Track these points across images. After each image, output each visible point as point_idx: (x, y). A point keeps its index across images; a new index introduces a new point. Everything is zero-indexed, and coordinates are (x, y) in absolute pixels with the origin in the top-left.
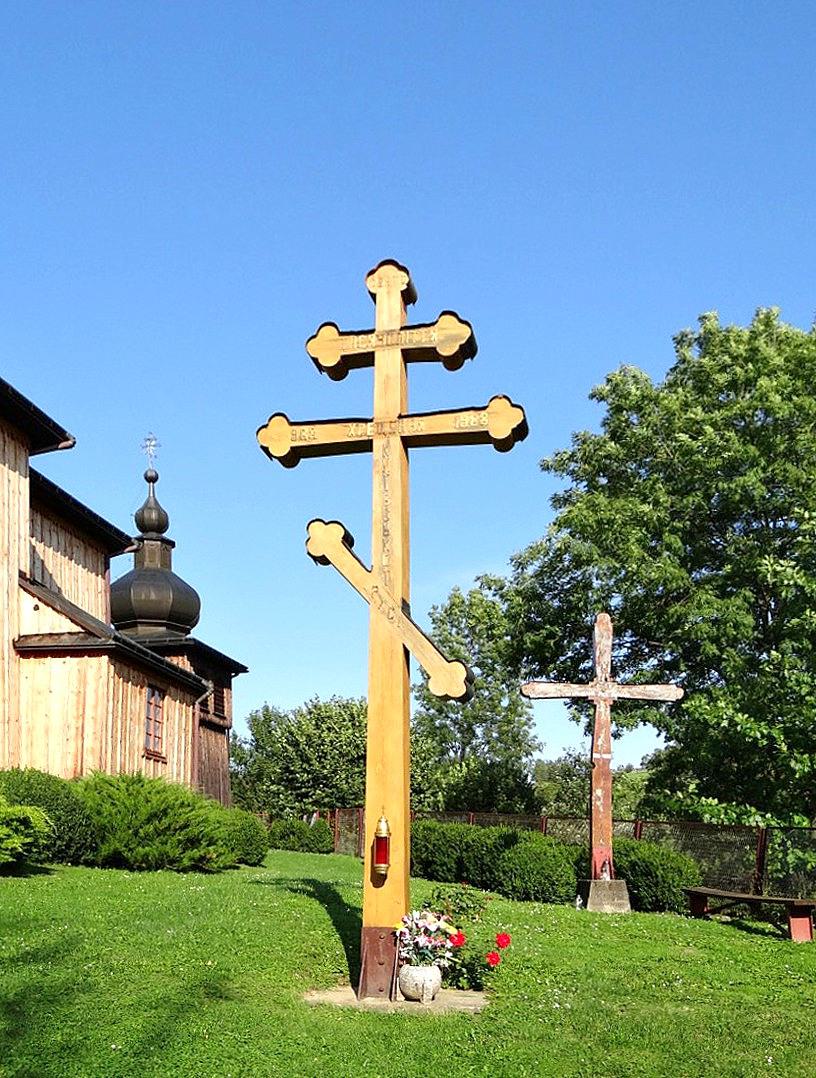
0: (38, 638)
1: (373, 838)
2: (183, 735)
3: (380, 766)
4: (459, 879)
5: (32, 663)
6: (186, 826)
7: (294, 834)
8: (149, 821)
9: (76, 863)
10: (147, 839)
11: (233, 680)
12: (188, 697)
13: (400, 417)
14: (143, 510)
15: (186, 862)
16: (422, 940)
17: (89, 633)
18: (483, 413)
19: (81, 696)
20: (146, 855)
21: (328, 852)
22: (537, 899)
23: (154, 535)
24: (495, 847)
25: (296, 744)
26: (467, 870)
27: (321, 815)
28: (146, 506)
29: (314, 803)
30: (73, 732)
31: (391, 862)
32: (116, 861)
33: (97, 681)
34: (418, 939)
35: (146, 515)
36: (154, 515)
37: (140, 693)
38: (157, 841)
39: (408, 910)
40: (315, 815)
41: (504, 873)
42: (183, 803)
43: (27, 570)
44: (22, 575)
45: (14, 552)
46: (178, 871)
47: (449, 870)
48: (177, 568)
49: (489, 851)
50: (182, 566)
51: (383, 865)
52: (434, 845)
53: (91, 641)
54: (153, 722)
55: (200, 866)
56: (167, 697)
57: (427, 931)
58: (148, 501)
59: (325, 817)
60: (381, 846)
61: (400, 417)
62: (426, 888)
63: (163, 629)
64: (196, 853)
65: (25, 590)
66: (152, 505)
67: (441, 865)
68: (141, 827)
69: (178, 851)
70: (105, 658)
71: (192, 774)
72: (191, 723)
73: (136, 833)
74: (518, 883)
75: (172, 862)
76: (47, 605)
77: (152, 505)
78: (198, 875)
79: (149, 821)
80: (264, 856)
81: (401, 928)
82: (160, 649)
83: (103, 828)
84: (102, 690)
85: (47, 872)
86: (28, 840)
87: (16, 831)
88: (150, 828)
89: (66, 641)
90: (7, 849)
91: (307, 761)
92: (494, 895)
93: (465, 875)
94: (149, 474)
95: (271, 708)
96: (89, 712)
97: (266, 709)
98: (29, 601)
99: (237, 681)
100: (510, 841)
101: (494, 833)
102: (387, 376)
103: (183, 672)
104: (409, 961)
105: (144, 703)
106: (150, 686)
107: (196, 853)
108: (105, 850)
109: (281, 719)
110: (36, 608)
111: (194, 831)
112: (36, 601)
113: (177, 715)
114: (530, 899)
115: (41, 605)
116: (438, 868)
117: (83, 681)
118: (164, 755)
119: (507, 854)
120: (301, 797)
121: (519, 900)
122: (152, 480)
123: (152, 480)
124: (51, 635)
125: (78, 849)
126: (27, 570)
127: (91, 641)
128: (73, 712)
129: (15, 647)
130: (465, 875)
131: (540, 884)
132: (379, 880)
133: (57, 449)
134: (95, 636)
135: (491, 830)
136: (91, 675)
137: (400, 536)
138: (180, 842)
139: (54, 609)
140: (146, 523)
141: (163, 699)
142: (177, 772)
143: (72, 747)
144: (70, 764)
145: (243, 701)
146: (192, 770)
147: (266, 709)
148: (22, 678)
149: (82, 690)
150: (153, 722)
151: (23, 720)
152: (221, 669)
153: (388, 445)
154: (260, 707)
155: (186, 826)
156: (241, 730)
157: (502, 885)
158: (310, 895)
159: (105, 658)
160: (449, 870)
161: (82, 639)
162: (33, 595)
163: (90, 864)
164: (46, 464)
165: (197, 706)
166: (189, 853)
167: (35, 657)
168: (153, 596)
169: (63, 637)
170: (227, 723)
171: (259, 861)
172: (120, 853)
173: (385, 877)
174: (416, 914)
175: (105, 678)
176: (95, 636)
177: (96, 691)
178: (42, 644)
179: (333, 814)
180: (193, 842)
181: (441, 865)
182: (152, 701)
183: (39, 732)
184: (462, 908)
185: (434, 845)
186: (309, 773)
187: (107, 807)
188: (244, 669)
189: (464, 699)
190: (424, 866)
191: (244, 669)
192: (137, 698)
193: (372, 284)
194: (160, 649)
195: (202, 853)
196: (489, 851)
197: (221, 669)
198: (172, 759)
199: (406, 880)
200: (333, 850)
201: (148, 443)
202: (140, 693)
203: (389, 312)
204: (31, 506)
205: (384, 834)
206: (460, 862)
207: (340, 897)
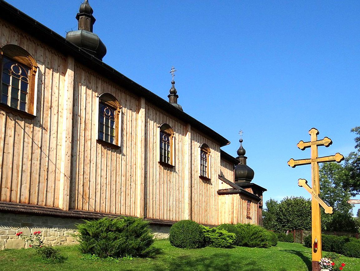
0: (222, 190)
1: (314, 242)
2: (255, 212)
3: (315, 228)
4: (332, 251)
5: (221, 197)
6: (261, 236)
7: (282, 237)
8: (253, 235)
9: (238, 245)
10: (252, 240)
11: (263, 193)
12: (256, 202)
13: (317, 158)
14: (239, 150)
15: (261, 245)
16: (325, 264)
17: (234, 189)
18: (334, 156)
19: (233, 204)
20: (253, 243)
21: (292, 242)
22: (355, 257)
23: (242, 156)
24: (342, 242)
25: (282, 211)
26: (334, 248)
27: (290, 231)
28: (240, 149)
29: (288, 227)
30: (231, 212)
31: (318, 248)
32: (246, 245)
33: (236, 200)
34: (324, 264)
35: (240, 151)
36: (242, 151)
37: (246, 202)
38: (254, 240)
39: (322, 258)
40: (287, 231)
41: (345, 250)
42: (260, 231)
43: (220, 174)
44: (219, 175)
45: (217, 171)
46: (260, 248)
47: (329, 248)
48: (248, 164)
49: (341, 243)
50: (249, 163)
51: (316, 248)
52: (324, 241)
53: (235, 191)
54: (248, 209)
55: (264, 246)
56: (251, 203)
57: (326, 262)
58: (240, 148)
59: (291, 232)
60: (316, 244)
61: (317, 158)
62: (325, 253)
63: (245, 181)
64: (263, 243)
65: (220, 179)
66: (241, 148)
67: (327, 247)
68: (251, 237)
69: (259, 243)
70: (238, 194)
71: (257, 221)
72: (257, 208)
73: (250, 238)
74: (348, 252)
75: (258, 245)
76: (225, 182)
77: (241, 148)
78: (264, 249)
79: (253, 235)
80: (277, 243)
81: (320, 261)
82: (246, 187)
83: (242, 237)
84: (238, 202)
85: (234, 247)
86: (232, 240)
87: (230, 239)
88: (253, 237)
89: (229, 191)
90: (229, 243)
91: (285, 216)
92: (342, 255)
93: (334, 249)
94: (241, 140)
95: (272, 199)
96: (235, 208)
97: (271, 200)
98: (220, 181)
99: (264, 193)
100: (347, 240)
101: (342, 238)
102: (314, 151)
103: (250, 194)
104: (322, 268)
105: (246, 205)
106: (248, 200)
107: (263, 243)
108: (243, 242)
109: (275, 203)
110: (222, 183)
111: (263, 237)
112: (222, 181)
113: (254, 206)
114: (352, 257)
115: (223, 182)
116: (326, 247)
117: (233, 200)
118: (251, 217)
119: (345, 245)
120: (284, 226)
121: (349, 257)
122: (241, 141)
123: (241, 141)
124: (226, 189)
125: (238, 242)
126: (220, 174)
127: (235, 191)
128: (231, 208)
129: (218, 193)
130: (334, 249)
131: (355, 253)
132: (315, 251)
133: (226, 145)
134: (236, 189)
135: (341, 237)
136: (235, 198)
137: (317, 179)
138: (260, 240)
139: (226, 183)
140: (240, 153)
141: (250, 203)
142: (254, 222)
143: (231, 216)
144: (230, 220)
145: (266, 198)
146: (257, 220)
147: (271, 200)
148: (219, 200)
149: (233, 202)
150: (248, 209)
151: (219, 210)
152: (259, 190)
153: (314, 164)
154: (269, 199)
155: (261, 236)
156: (265, 207)
157: (344, 253)
158: (296, 254)
159: (238, 194)
160: (329, 248)
161: (232, 190)
162: (222, 180)
163: (240, 246)
164: (223, 148)
165: (258, 204)
166: (262, 243)
167: (222, 195)
168: (242, 172)
169: (228, 190)
170: (261, 205)
171: (276, 245)
172: (247, 243)
173: (317, 251)
174: (323, 258)
175: (238, 200)
176: (236, 189)
177: (236, 203)
178: (224, 192)
179: (293, 231)
180: (263, 240)
181: (327, 247)
182: (248, 204)
183: (223, 213)
184: (333, 258)
185: (324, 241)
186: (285, 219)
187: (243, 232)
188: (266, 190)
189: (333, 213)
190: (323, 249)
191: (266, 190)
192: (245, 203)
193: (310, 133)
194: (246, 187)
195: (265, 243)
196: (341, 243)
197: (259, 190)
198: (253, 218)
199: (321, 252)
200: (294, 242)
201: (240, 132)
202: (246, 202)
203: (313, 137)
204: (221, 159)
205: (316, 242)
206: (332, 246)
207: (303, 255)
